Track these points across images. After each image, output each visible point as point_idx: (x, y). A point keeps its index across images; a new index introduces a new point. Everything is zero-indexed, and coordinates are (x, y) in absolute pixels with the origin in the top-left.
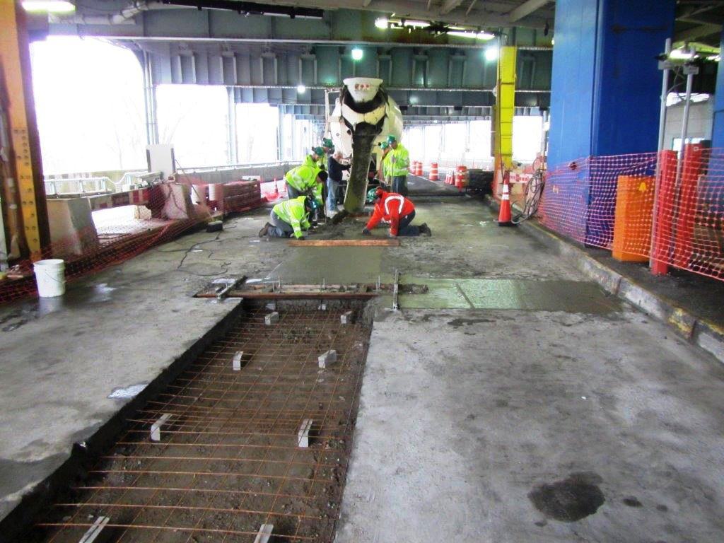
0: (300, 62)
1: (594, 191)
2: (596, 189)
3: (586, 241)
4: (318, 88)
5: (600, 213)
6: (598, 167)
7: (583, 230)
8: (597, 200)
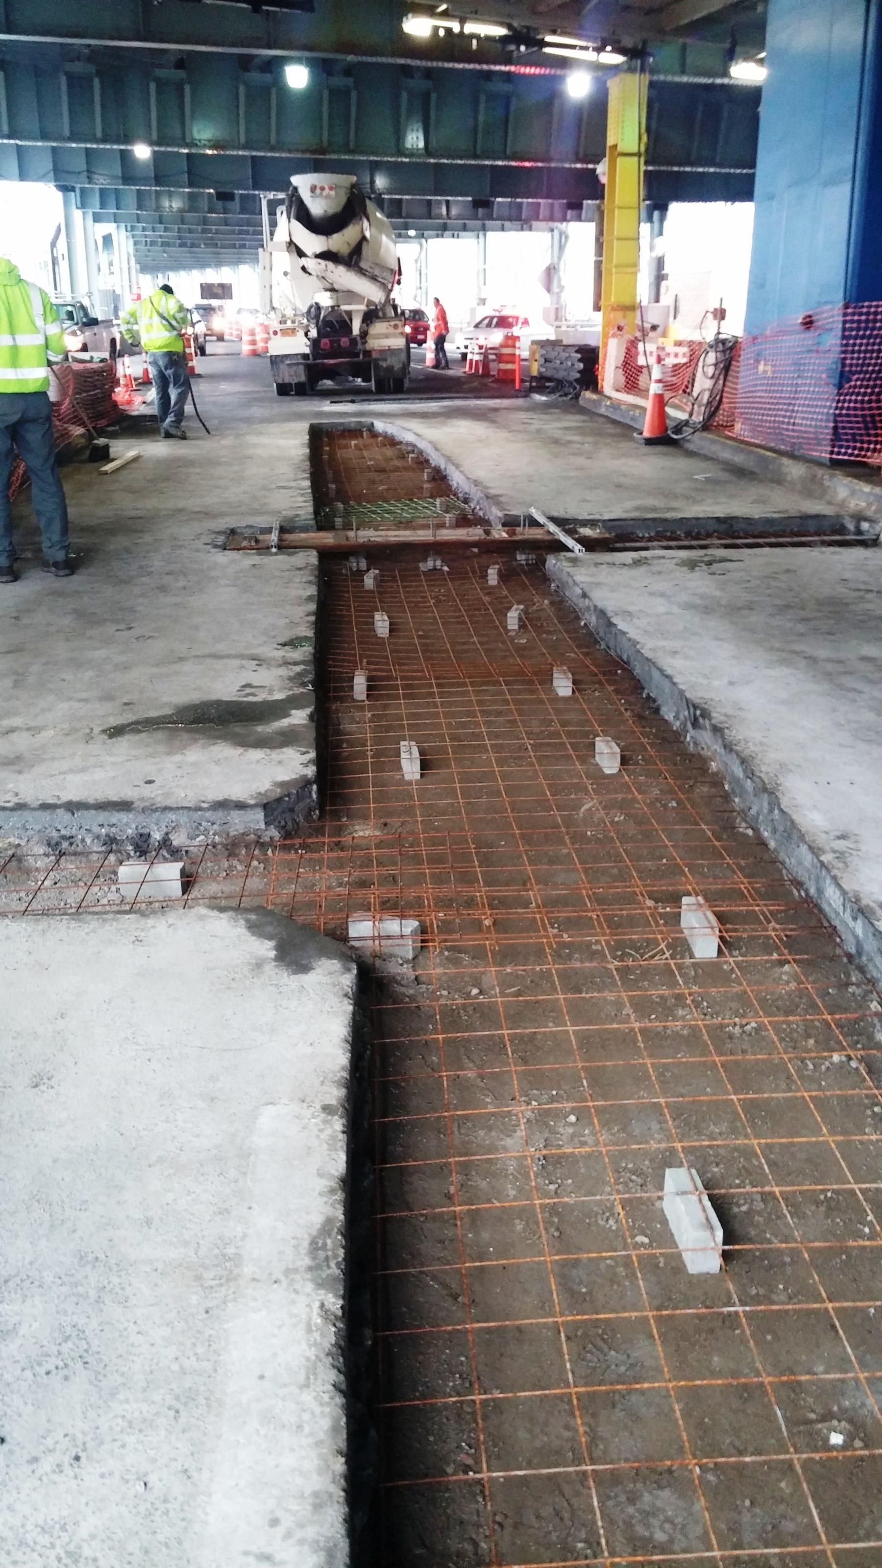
0: (153, 86)
1: (851, 365)
2: (854, 362)
3: (832, 453)
4: (101, 146)
5: (862, 402)
6: (859, 321)
7: (827, 433)
8: (857, 380)
